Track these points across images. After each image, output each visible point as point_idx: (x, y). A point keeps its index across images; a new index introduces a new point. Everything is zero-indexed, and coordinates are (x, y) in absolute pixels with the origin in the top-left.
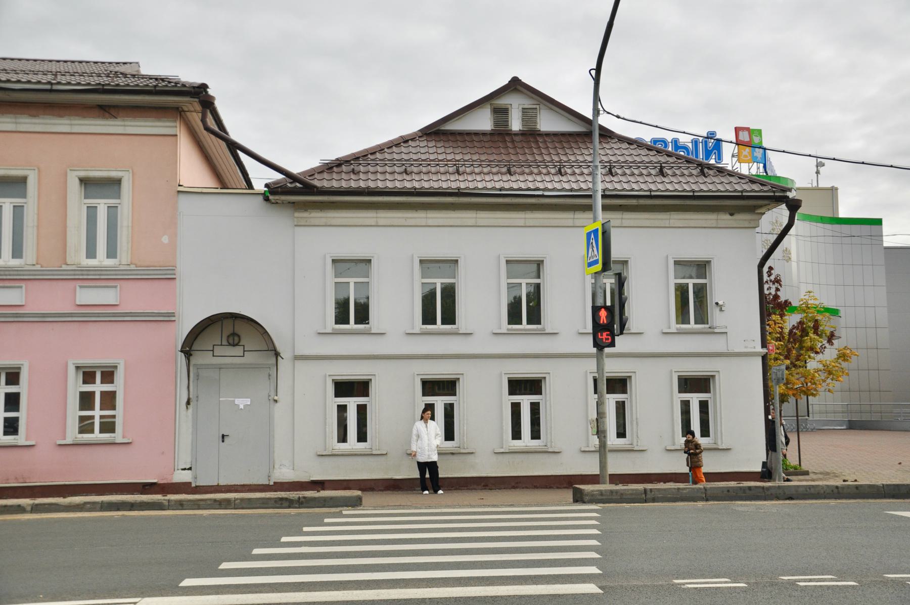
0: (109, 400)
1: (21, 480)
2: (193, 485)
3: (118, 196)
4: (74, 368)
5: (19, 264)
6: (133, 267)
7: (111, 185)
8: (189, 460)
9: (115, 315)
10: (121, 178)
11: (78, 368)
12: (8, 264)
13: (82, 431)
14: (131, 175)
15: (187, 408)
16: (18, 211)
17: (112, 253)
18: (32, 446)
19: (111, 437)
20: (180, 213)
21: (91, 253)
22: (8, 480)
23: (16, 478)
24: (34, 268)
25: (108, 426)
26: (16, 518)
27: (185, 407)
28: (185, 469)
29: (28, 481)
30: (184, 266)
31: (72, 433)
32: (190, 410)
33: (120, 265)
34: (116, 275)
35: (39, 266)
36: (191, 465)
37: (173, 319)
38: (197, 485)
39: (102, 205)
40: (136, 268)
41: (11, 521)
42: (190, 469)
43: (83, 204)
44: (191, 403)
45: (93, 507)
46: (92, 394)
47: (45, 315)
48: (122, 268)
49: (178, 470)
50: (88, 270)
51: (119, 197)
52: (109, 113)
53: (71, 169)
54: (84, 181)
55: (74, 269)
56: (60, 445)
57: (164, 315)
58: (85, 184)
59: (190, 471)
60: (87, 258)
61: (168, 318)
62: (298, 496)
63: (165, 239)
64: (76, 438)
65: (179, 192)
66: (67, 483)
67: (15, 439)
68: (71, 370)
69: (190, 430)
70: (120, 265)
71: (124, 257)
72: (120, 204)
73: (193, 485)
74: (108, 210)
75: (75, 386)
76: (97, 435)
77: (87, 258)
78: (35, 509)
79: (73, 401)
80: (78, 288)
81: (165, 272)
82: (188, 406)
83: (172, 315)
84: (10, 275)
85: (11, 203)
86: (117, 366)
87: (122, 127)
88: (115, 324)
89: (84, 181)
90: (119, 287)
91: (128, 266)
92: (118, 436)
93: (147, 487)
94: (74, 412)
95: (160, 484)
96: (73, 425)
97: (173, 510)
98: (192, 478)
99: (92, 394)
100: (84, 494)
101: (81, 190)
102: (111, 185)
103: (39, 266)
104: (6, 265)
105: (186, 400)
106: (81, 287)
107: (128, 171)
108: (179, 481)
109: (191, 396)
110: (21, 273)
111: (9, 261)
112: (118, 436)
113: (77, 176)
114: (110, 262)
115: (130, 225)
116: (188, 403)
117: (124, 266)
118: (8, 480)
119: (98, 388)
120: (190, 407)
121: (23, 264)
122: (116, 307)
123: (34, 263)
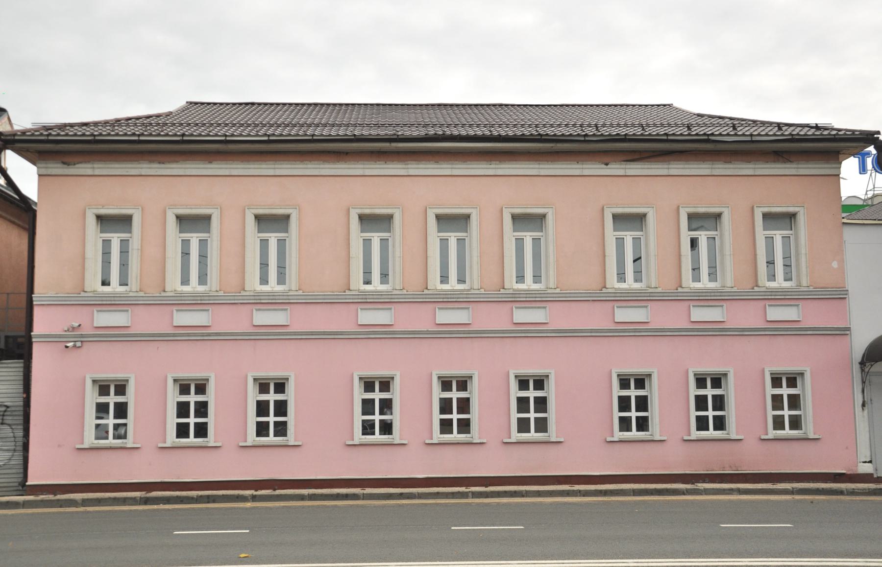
0: (386, 405)
1: (734, 468)
2: (875, 476)
3: (130, 231)
4: (91, 382)
5: (386, 289)
6: (811, 289)
7: (636, 220)
8: (868, 454)
9: (469, 332)
10: (393, 215)
11: (94, 381)
12: (377, 289)
13: (179, 436)
14: (219, 211)
15: (863, 409)
16: (124, 243)
17: (281, 280)
18: (219, 447)
19: (283, 440)
20: (845, 242)
21: (264, 280)
22: (724, 468)
23: (730, 467)
24: (733, 290)
25: (387, 428)
26: (720, 498)
27: (861, 409)
28: (865, 462)
29: (739, 469)
30: (852, 285)
31: (90, 438)
32: (866, 412)
33: (210, 291)
34: (181, 300)
35: (483, 290)
36: (871, 458)
37: (848, 332)
38: (879, 476)
39: (194, 239)
40: (144, 295)
41: (669, 501)
42: (870, 462)
43: (360, 238)
44: (866, 405)
45: (636, 493)
46: (187, 404)
47: (61, 336)
48: (395, 292)
49: (860, 462)
50: (181, 295)
51: (287, 232)
52: (783, 157)
53: (430, 207)
54: (100, 218)
55: (171, 295)
56: (78, 449)
57: (840, 329)
58: (258, 220)
59: (870, 464)
60: (260, 284)
61: (844, 332)
62: (307, 493)
63: (835, 265)
64: (254, 441)
65: (844, 223)
66: (772, 472)
67: (646, 435)
68: (89, 384)
69: (867, 429)
70: (210, 291)
71: (292, 282)
72: (288, 237)
73: (875, 476)
74: (278, 243)
75: (174, 397)
76: (787, 432)
77: (260, 284)
78: (254, 498)
79: (172, 410)
80: (254, 311)
81: (627, 295)
82: (864, 408)
83: (849, 329)
84: (714, 296)
85: (455, 236)
86: (208, 379)
87: (405, 170)
88: (268, 342)
89: (100, 218)
90: (289, 309)
91: (808, 288)
92: (129, 442)
93: (837, 477)
94: (173, 420)
95: (848, 474)
96: (172, 431)
97: (129, 505)
98: (874, 470)
99: (187, 404)
100: (45, 493)
101: (177, 226)
102: (123, 222)
103: (483, 290)
104: (114, 291)
105: (861, 402)
106: (177, 311)
107: (552, 208)
108: (863, 472)
109: (866, 399)
110: (724, 294)
111: (116, 288)
112: (129, 442)
113: (611, 212)
114: (201, 289)
115: (479, 255)
116: (863, 405)
117: (729, 288)
118: (724, 468)
119: (112, 399)
120: (866, 408)
121: (128, 290)
122: (391, 327)
123: (402, 288)
